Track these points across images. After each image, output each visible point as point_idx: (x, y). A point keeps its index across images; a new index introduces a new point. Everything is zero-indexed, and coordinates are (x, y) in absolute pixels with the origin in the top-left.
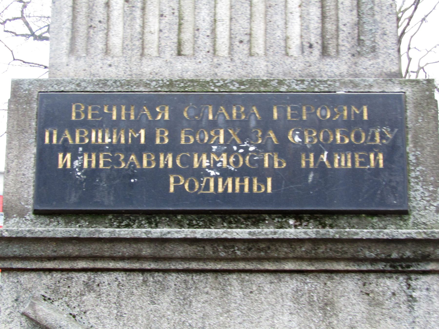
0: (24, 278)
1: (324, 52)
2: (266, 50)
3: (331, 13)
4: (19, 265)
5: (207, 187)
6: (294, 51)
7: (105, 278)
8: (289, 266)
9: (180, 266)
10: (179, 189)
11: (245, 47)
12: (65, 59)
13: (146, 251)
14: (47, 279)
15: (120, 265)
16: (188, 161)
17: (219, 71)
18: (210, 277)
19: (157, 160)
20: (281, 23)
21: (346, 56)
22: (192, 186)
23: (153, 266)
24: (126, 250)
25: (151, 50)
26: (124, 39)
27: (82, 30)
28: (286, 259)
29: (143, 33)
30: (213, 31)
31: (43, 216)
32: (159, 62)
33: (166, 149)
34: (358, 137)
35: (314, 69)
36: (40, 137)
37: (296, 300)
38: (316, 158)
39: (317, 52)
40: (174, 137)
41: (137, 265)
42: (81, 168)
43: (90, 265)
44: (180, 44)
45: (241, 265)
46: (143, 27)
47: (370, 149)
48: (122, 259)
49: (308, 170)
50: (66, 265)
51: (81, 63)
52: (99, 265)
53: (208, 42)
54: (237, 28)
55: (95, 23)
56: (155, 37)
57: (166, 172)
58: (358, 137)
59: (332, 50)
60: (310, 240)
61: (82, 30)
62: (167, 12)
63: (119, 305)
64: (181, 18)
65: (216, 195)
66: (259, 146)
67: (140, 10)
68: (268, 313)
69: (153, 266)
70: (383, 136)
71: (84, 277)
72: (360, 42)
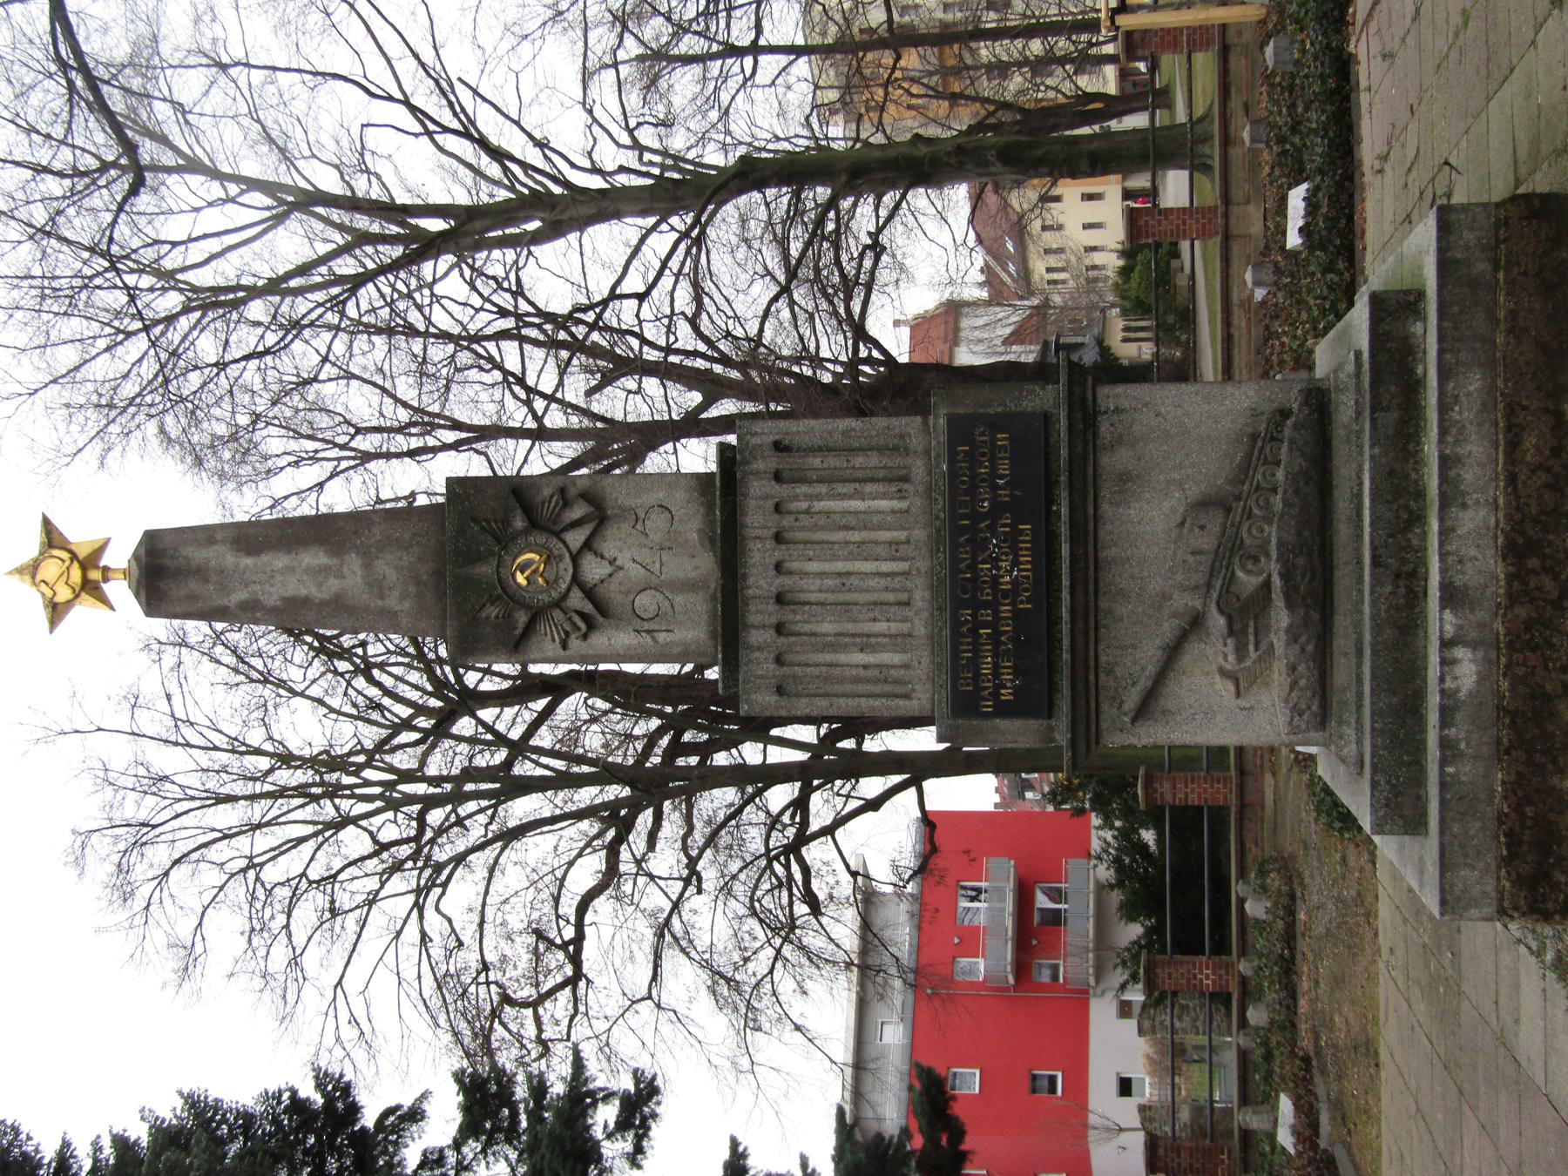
0: (1104, 725)
1: (905, 479)
2: (903, 529)
3: (869, 473)
4: (1093, 728)
5: (1027, 577)
6: (904, 505)
7: (1103, 659)
8: (1091, 510)
9: (1092, 598)
10: (1029, 600)
11: (902, 548)
12: (915, 702)
13: (1080, 625)
14: (1105, 707)
15: (1092, 647)
16: (1006, 594)
17: (923, 570)
18: (1101, 574)
20: (880, 517)
21: (909, 461)
22: (1026, 590)
23: (1092, 620)
24: (1080, 640)
25: (905, 627)
26: (896, 651)
27: (887, 688)
28: (1085, 512)
29: (891, 636)
30: (887, 575)
31: (1068, 181)
32: (916, 621)
33: (996, 613)
34: (983, 455)
35: (921, 488)
36: (987, 716)
37: (1118, 504)
38: (1001, 488)
39: (905, 486)
40: (986, 605)
41: (1092, 633)
42: (1012, 681)
44: (899, 603)
45: (1091, 548)
46: (885, 636)
47: (993, 445)
48: (1087, 644)
49: (1012, 496)
50: (1093, 690)
51: (917, 687)
52: (1092, 663)
53: (898, 579)
55: (882, 677)
56: (893, 625)
57: (1015, 611)
58: (983, 455)
59: (903, 472)
60: (1071, 494)
61: (887, 688)
62: (871, 615)
63: (1125, 647)
64: (875, 603)
65: (1033, 570)
66: (993, 536)
68: (1130, 527)
69: (1092, 620)
70: (982, 434)
71: (1102, 677)
72: (895, 449)
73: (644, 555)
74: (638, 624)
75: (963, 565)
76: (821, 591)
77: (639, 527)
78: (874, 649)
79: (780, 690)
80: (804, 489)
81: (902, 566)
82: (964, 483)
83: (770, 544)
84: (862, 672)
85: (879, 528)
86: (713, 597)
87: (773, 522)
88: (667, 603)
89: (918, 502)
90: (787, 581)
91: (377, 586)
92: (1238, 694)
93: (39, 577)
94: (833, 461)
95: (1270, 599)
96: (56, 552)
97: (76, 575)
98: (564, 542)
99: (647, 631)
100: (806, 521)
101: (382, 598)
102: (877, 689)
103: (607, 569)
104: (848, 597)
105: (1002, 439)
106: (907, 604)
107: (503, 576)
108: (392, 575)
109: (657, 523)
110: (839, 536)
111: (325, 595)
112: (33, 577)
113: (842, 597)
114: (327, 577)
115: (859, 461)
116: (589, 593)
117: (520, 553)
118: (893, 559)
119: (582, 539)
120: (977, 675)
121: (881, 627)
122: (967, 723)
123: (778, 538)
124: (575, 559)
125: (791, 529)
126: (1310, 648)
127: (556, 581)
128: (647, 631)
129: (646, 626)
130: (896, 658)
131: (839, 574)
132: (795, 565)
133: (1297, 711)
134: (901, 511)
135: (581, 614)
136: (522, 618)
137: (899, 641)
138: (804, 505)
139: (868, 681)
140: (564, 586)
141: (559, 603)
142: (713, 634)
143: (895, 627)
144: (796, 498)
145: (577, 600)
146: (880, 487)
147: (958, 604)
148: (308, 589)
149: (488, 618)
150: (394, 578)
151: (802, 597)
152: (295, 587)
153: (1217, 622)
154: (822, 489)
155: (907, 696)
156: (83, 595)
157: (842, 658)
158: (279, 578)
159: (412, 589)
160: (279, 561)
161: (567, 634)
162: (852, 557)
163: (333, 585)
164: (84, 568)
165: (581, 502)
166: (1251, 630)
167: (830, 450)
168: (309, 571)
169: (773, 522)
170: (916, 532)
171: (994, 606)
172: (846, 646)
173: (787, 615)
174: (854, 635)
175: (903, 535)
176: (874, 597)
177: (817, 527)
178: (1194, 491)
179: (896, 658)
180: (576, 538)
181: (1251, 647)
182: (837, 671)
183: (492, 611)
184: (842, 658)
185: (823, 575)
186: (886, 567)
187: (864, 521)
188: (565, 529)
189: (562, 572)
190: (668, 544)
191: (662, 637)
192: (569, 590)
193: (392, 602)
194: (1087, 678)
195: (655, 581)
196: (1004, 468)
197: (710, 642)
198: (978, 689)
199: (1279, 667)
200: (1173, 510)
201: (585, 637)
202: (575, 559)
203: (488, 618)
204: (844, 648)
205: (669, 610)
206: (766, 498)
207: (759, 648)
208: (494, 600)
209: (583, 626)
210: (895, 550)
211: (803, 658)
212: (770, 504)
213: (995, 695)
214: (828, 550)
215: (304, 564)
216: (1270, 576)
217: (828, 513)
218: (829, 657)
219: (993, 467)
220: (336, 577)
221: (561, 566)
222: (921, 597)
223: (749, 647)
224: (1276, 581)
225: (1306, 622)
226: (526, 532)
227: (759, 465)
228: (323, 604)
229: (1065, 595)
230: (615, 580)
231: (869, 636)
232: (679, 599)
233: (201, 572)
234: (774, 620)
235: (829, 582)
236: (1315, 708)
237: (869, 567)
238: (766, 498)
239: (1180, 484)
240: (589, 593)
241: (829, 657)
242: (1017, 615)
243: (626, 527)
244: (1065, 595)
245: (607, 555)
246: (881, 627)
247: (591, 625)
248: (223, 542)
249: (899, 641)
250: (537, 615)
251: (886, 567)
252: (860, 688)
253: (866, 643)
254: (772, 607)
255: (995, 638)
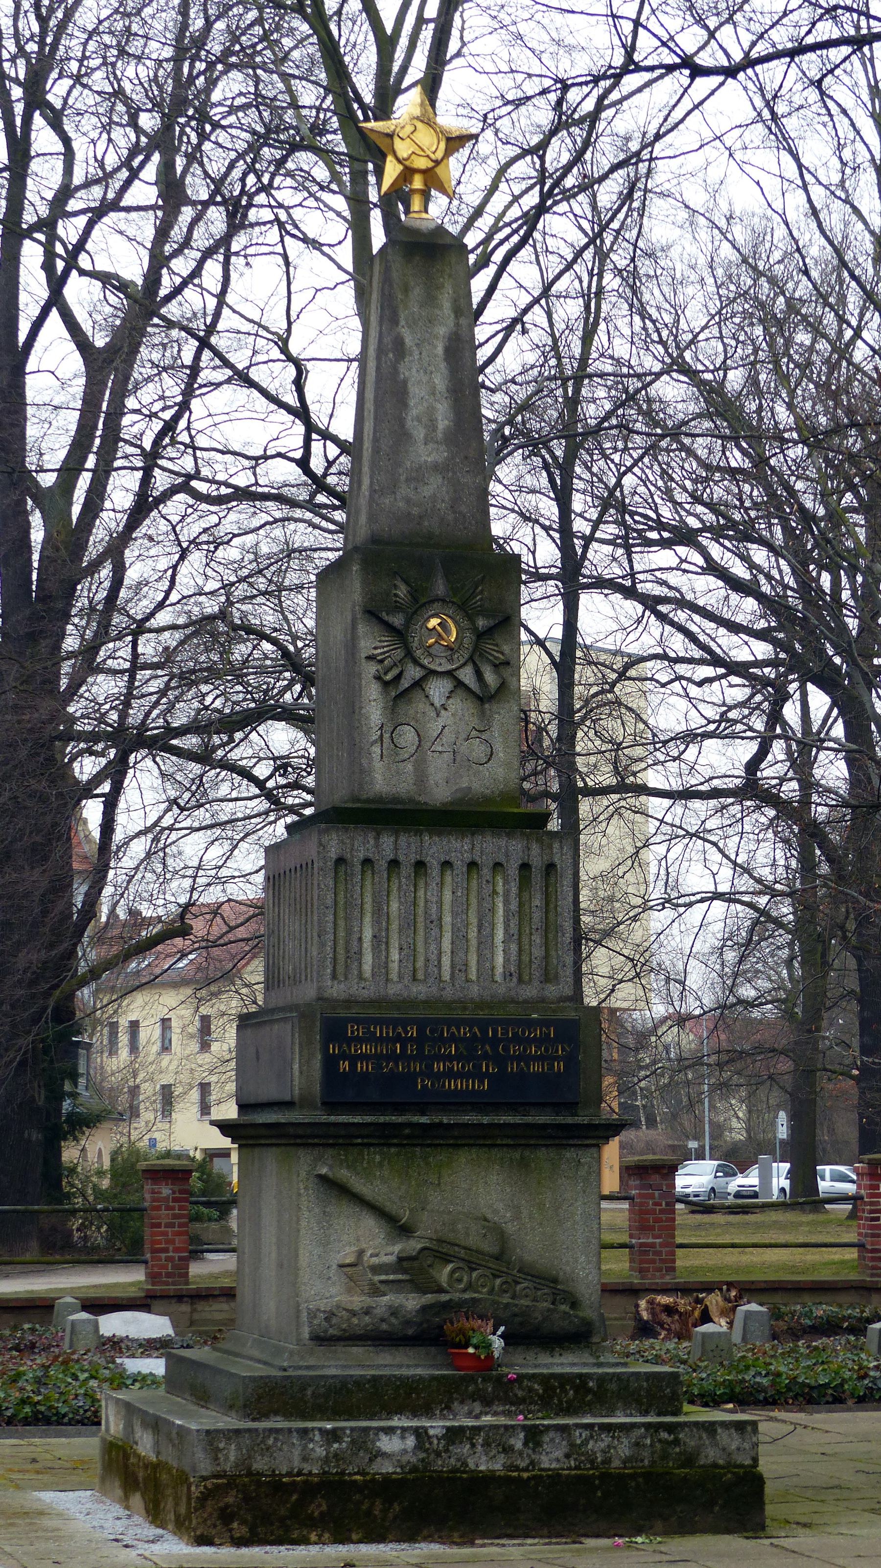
1: (520, 981)
2: (478, 978)
6: (498, 978)
10: (424, 1087)
12: (329, 983)
16: (430, 1067)
19: (409, 1066)
21: (536, 983)
27: (341, 957)
29: (387, 963)
30: (439, 961)
32: (400, 986)
33: (412, 1058)
35: (513, 993)
39: (515, 980)
43: (322, 1141)
51: (342, 986)
54: (457, 959)
55: (352, 954)
58: (546, 1050)
61: (341, 957)
67: (765, 1475)
73: (448, 737)
74: (388, 728)
75: (454, 1029)
76: (426, 901)
77: (474, 733)
78: (376, 948)
79: (340, 861)
80: (514, 890)
81: (446, 975)
82: (523, 1033)
83: (467, 857)
84: (356, 936)
85: (480, 955)
86: (411, 800)
87: (486, 862)
88: (406, 756)
89: (502, 990)
90: (435, 872)
91: (418, 477)
92: (341, 1266)
93: (419, 125)
94: (537, 916)
95: (425, 1293)
96: (443, 145)
97: (422, 163)
98: (464, 665)
99: (381, 736)
100: (487, 889)
101: (407, 480)
102: (341, 951)
103: (437, 703)
104: (421, 926)
105: (559, 1066)
106: (415, 979)
107: (435, 605)
108: (427, 491)
109: (478, 750)
110: (474, 920)
111: (409, 423)
112: (417, 118)
113: (420, 919)
114: (426, 426)
115: (537, 939)
116: (418, 684)
117: (456, 623)
118: (453, 966)
119: (467, 681)
120: (359, 1040)
121: (395, 955)
122: (317, 1029)
123: (472, 865)
124: (450, 674)
125: (480, 877)
126: (384, 1326)
127: (430, 655)
128: (381, 736)
129: (387, 736)
130: (367, 968)
131: (440, 919)
132: (448, 879)
133: (330, 1316)
134: (493, 975)
135: (399, 677)
136: (397, 620)
137: (382, 966)
138: (500, 888)
139: (347, 942)
140: (425, 662)
141: (409, 654)
142: (379, 799)
143: (394, 966)
144: (506, 882)
145: (413, 673)
146: (514, 957)
147: (421, 1024)
148: (416, 408)
149: (396, 587)
150: (426, 494)
151: (421, 884)
152: (417, 393)
153: (414, 1246)
154: (514, 906)
155: (334, 977)
156: (401, 167)
157: (368, 919)
158: (425, 379)
159: (415, 511)
160: (440, 382)
161: (381, 661)
162: (455, 930)
163: (419, 433)
164: (427, 173)
165: (500, 681)
166: (400, 1277)
167: (547, 912)
168: (431, 410)
169: (486, 862)
170: (476, 988)
171: (420, 1057)
172: (379, 922)
173: (406, 870)
174: (387, 929)
175: (473, 977)
176: (420, 948)
177: (481, 900)
178: (511, 1228)
179: (367, 968)
180: (467, 675)
181: (383, 1277)
182: (356, 913)
183: (402, 591)
184: (368, 919)
185: (440, 903)
186: (446, 961)
187: (485, 943)
188: (475, 664)
189: (437, 661)
190: (458, 758)
191: (376, 749)
192: (423, 666)
193: (404, 491)
194: (357, 1137)
195: (426, 745)
196: (535, 1067)
197: (371, 795)
198: (349, 1041)
199: (357, 1301)
200: (496, 1212)
201: (378, 678)
202: (450, 674)
203: (396, 587)
204: (376, 921)
205: (401, 758)
206: (507, 855)
207: (377, 846)
208: (414, 594)
209: (388, 677)
210: (459, 968)
211: (368, 883)
212: (502, 859)
213: (344, 1056)
214: (460, 909)
215: (439, 406)
216: (447, 1292)
217: (493, 910)
218: (368, 907)
219: (537, 1058)
220: (426, 438)
221: (443, 661)
222: (420, 991)
223: (377, 838)
224: (444, 1297)
225: (408, 1323)
226: (475, 629)
227: (535, 849)
228: (402, 423)
229: (369, 1119)
230: (428, 708)
231: (387, 943)
232: (409, 767)
233: (430, 300)
234: (401, 858)
235: (434, 909)
236: (331, 1331)
237: (446, 945)
238: (507, 855)
239: (517, 1217)
240: (418, 684)
241: (368, 907)
242: (411, 1077)
243: (475, 722)
244: (369, 1119)
245: (451, 701)
246: (395, 955)
247: (386, 684)
248: (457, 325)
249: (382, 966)
250: (400, 635)
251: (446, 961)
252: (341, 934)
253: (380, 942)
254: (413, 858)
255: (392, 1057)
